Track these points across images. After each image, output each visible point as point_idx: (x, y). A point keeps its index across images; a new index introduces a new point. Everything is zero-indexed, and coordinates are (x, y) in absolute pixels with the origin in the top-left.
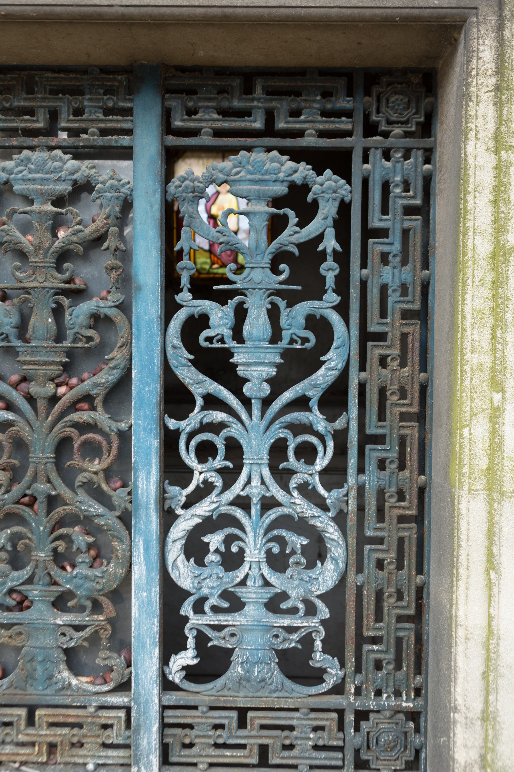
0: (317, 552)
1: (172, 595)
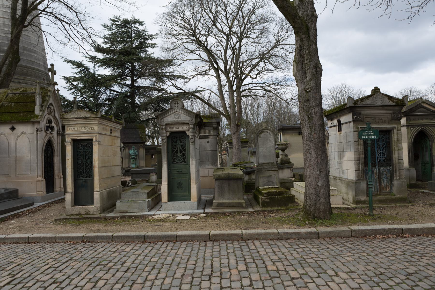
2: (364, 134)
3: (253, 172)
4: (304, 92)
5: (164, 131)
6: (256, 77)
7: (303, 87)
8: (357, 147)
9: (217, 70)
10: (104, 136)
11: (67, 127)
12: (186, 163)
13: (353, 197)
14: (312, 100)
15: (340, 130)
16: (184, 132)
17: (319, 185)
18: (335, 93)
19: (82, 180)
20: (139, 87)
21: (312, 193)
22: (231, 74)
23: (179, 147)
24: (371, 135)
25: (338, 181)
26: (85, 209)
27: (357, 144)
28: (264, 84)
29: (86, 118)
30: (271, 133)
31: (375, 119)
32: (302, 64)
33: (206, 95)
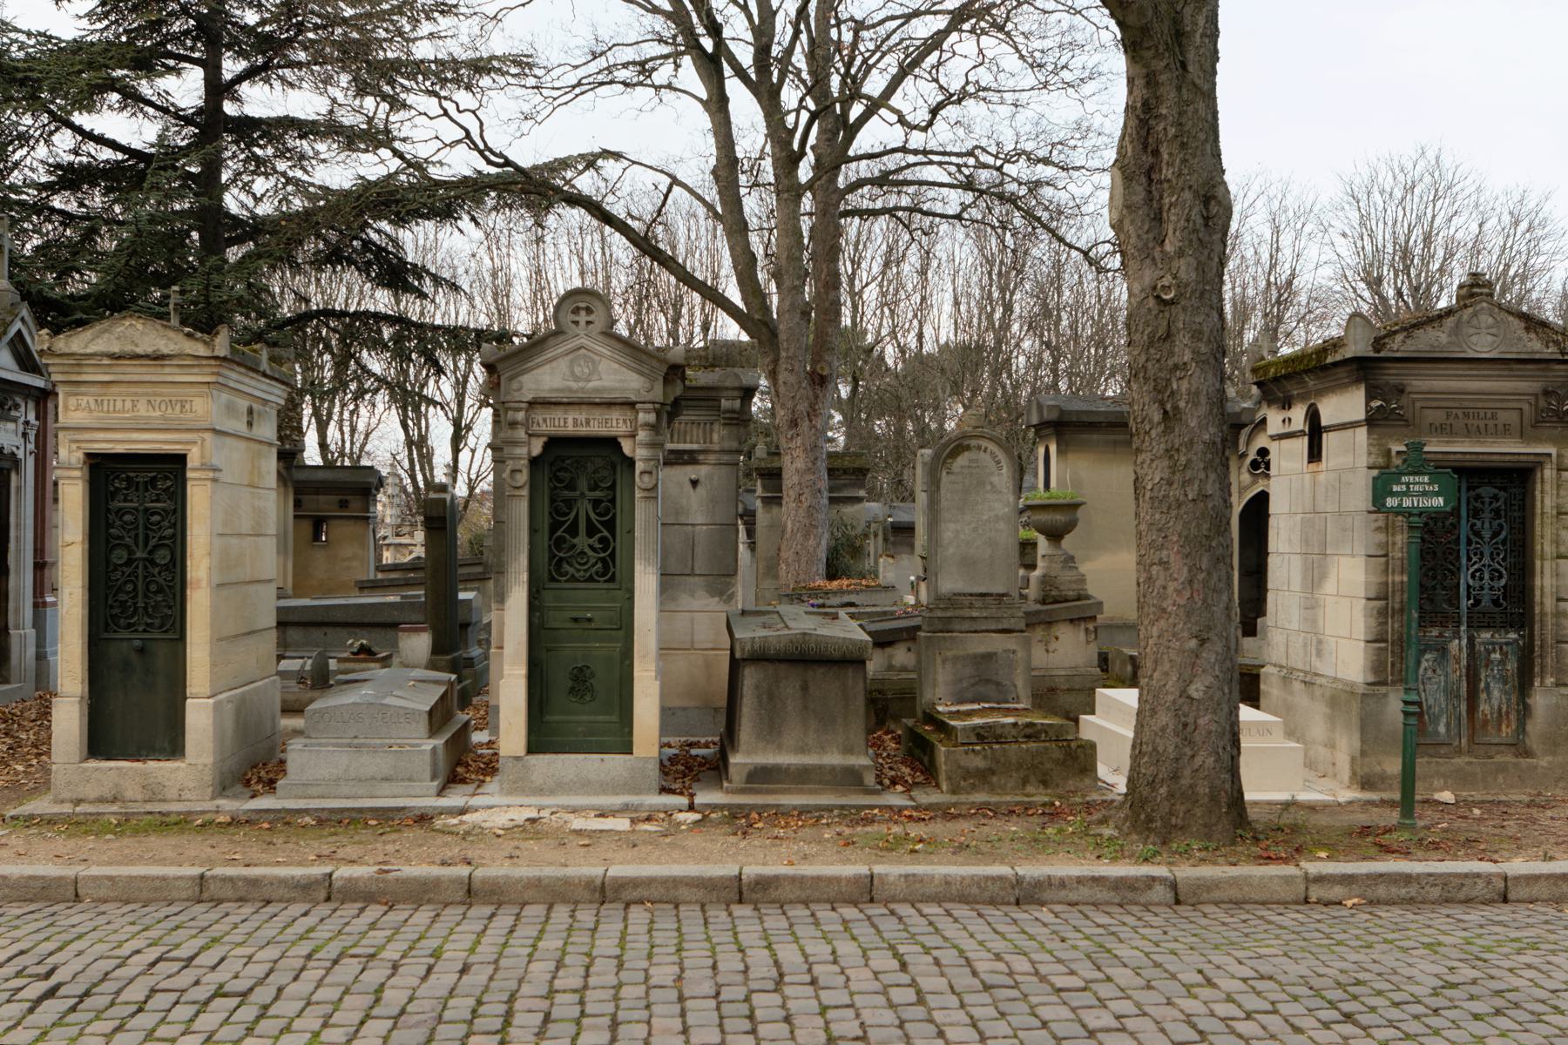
0: (1501, 577)
1: (1469, 587)
2: (1395, 488)
3: (910, 634)
4: (1151, 302)
5: (521, 434)
6: (930, 123)
7: (1147, 281)
8: (1381, 537)
9: (712, 65)
10: (228, 440)
11: (68, 395)
12: (612, 579)
13: (1353, 760)
14: (1182, 339)
15: (1315, 454)
16: (612, 443)
17: (1195, 695)
18: (1377, 197)
19: (123, 644)
20: (247, 128)
21: (1163, 729)
22: (790, 96)
23: (584, 509)
24: (1424, 494)
25: (1297, 686)
26: (145, 775)
27: (1381, 523)
28: (970, 154)
29: (158, 357)
30: (1001, 456)
31: (1466, 415)
32: (1150, 180)
33: (632, 192)
